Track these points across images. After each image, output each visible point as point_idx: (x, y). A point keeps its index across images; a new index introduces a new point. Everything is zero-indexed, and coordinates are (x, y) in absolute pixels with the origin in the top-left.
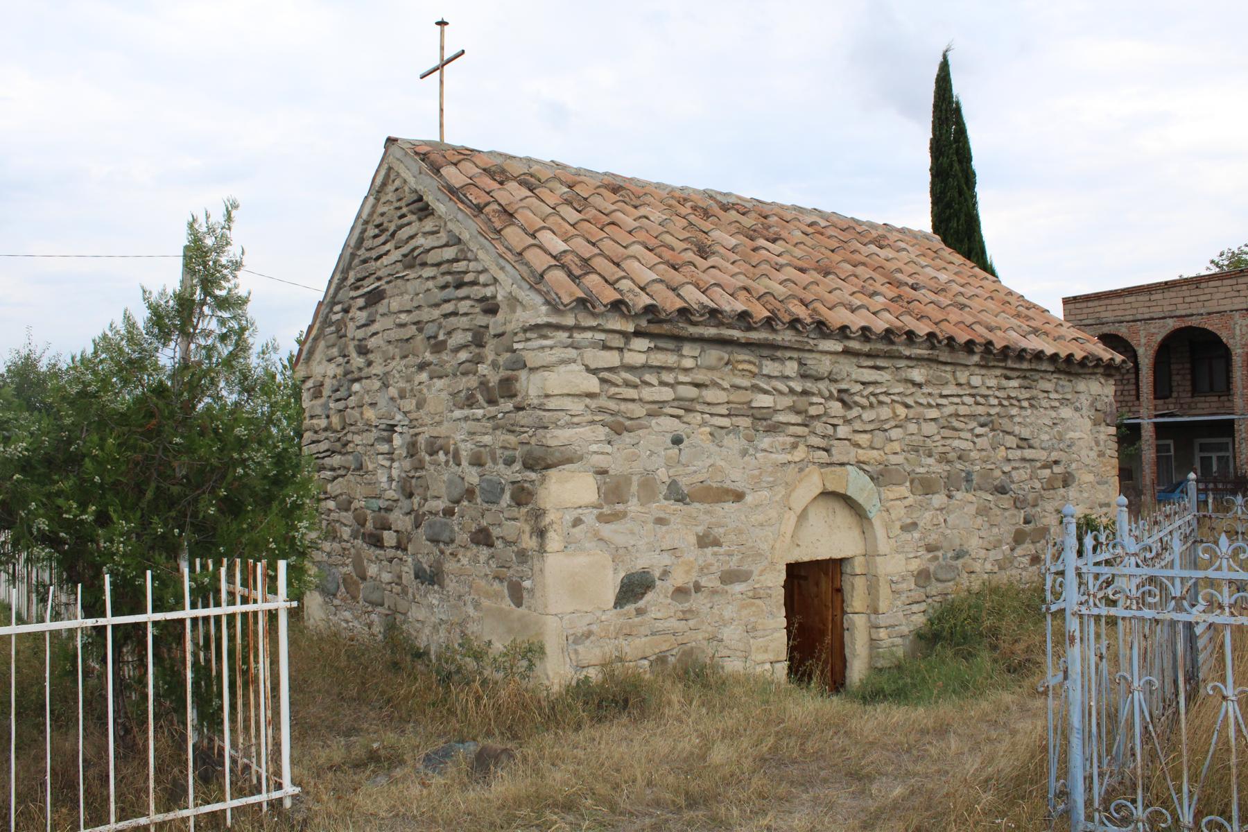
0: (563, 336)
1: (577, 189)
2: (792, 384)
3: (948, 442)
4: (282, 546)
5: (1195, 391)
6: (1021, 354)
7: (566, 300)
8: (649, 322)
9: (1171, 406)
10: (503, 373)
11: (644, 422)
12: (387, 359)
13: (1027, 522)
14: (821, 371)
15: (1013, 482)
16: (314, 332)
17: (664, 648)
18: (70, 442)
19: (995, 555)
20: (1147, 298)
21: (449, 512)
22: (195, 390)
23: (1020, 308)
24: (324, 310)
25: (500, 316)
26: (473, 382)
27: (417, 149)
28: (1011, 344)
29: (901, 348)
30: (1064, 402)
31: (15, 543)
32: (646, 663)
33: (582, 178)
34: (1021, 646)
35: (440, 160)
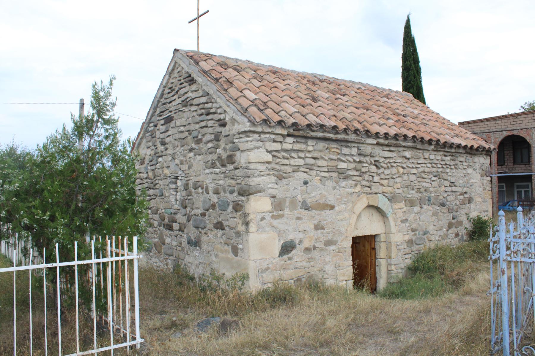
0: (256, 136)
1: (258, 72)
2: (355, 158)
3: (421, 184)
4: (133, 230)
5: (515, 163)
6: (451, 146)
7: (258, 120)
8: (294, 130)
9: (504, 169)
10: (229, 153)
11: (291, 174)
12: (174, 147)
13: (453, 219)
14: (367, 152)
15: (447, 201)
16: (141, 135)
17: (300, 275)
18: (36, 184)
19: (440, 233)
20: (494, 122)
21: (203, 215)
22: (93, 160)
23: (449, 126)
24: (145, 125)
25: (227, 127)
26: (215, 157)
27: (188, 54)
28: (447, 141)
29: (401, 143)
30: (469, 166)
31: (13, 229)
32: (292, 281)
33: (259, 68)
34: (454, 273)
35: (199, 59)
